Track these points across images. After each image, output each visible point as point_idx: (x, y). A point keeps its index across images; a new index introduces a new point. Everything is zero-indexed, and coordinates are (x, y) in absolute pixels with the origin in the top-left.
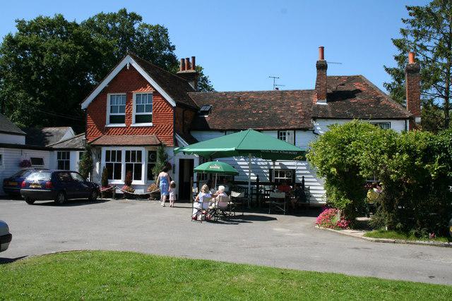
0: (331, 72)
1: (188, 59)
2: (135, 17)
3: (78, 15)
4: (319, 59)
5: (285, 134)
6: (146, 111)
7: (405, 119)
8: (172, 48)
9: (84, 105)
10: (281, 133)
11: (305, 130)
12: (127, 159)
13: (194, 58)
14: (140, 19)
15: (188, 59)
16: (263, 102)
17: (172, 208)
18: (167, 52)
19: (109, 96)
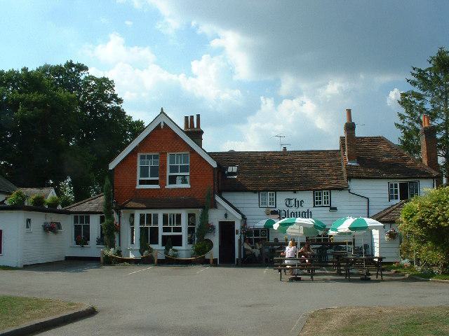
0: (359, 133)
1: (192, 117)
2: (81, 68)
3: (32, 67)
4: (346, 121)
5: (320, 193)
6: (151, 177)
7: (433, 178)
8: (119, 101)
9: (112, 166)
10: (317, 193)
11: (341, 189)
12: (142, 222)
13: (198, 116)
14: (86, 69)
15: (192, 117)
16: (290, 162)
17: (86, 306)
18: (114, 104)
19: (139, 155)
